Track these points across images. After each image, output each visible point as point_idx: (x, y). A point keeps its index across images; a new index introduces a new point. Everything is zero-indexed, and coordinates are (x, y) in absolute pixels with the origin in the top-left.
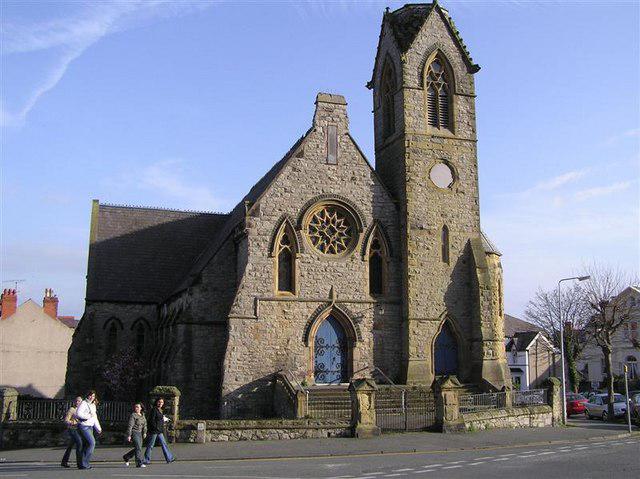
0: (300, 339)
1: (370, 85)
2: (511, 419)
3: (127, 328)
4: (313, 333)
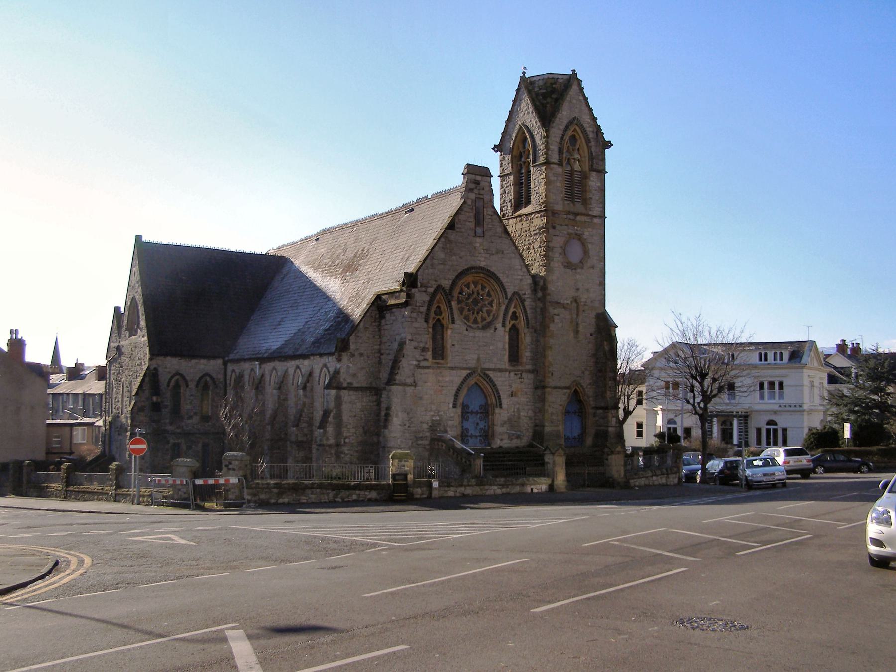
0: (451, 405)
1: (497, 148)
2: (654, 478)
3: (192, 385)
4: (460, 400)
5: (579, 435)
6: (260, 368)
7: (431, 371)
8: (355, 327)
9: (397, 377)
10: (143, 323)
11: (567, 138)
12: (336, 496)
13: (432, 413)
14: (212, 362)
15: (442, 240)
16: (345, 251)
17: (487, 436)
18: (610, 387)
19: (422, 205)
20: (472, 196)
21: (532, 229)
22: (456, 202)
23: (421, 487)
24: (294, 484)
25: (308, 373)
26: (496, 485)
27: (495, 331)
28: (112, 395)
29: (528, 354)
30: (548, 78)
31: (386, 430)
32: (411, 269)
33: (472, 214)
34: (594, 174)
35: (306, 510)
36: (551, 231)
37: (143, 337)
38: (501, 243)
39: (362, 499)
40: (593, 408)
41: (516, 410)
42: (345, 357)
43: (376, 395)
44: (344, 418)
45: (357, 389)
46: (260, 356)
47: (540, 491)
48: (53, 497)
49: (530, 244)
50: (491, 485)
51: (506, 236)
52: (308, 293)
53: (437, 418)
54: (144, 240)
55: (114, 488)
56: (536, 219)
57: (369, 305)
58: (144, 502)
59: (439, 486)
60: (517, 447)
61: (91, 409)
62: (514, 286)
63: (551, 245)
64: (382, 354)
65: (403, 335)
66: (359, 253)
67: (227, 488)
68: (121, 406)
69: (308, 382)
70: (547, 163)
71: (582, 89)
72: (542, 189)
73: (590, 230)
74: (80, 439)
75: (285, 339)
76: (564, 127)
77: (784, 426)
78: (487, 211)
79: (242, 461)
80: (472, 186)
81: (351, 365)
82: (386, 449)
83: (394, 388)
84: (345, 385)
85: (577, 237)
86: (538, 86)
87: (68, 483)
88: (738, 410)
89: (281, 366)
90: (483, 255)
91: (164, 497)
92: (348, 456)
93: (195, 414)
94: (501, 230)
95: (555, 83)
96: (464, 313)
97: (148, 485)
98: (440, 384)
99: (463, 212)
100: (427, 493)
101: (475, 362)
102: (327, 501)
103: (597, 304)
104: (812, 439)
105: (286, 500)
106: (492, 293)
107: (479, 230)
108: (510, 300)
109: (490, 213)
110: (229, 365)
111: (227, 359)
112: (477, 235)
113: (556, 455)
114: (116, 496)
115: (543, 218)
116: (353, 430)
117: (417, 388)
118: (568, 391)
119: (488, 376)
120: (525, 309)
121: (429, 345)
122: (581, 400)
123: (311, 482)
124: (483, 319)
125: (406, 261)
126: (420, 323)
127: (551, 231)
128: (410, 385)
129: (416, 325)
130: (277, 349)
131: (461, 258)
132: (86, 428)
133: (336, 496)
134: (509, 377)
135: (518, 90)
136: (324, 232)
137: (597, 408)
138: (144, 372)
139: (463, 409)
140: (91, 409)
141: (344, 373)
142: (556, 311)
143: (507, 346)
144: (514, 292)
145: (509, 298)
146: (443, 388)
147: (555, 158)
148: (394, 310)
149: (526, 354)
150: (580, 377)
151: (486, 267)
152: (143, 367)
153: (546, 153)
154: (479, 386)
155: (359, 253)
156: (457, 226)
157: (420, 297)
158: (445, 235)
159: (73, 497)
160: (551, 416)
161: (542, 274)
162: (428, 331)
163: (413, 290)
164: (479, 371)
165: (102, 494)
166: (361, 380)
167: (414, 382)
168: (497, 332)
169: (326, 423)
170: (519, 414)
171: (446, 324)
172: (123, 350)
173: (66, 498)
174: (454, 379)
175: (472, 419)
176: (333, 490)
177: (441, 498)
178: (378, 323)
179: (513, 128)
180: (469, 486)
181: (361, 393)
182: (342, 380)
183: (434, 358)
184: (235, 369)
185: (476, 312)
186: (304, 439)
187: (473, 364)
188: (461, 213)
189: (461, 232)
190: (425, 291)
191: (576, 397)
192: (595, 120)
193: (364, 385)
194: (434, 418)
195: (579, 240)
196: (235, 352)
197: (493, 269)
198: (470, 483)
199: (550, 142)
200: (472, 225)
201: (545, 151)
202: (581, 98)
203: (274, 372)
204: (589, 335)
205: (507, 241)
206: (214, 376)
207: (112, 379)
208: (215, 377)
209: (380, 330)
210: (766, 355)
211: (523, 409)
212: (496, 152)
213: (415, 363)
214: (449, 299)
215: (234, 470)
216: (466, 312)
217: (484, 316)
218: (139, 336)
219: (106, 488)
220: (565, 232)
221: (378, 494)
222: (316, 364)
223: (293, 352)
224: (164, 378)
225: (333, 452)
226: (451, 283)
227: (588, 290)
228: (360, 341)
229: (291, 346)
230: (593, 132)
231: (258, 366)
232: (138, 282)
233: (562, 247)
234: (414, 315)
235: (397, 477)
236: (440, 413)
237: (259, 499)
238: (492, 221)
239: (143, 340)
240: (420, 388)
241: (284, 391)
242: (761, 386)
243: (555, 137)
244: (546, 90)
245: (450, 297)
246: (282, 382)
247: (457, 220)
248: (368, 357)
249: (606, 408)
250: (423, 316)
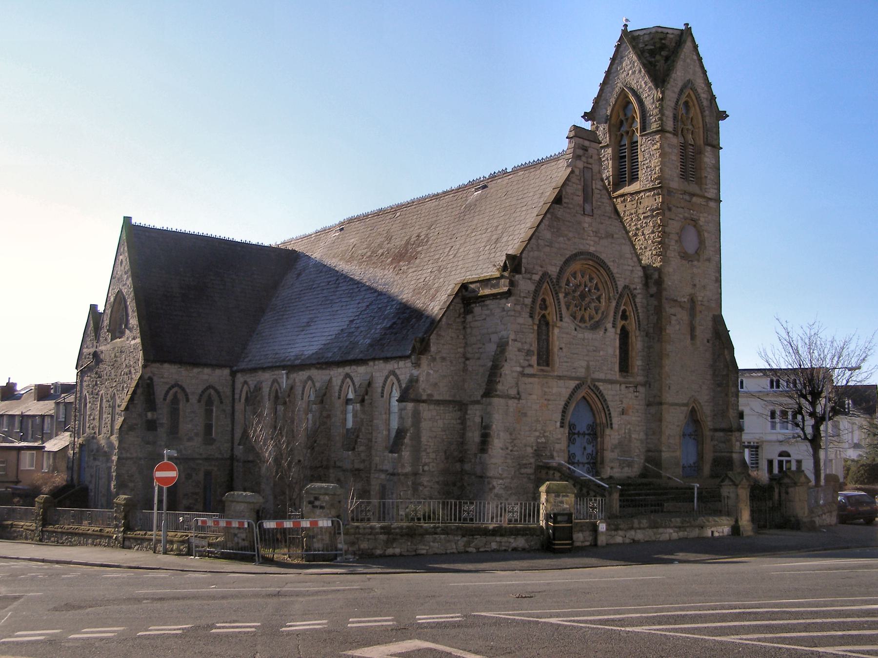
0: (558, 424)
3: (193, 399)
4: (568, 418)
5: (694, 463)
6: (288, 378)
7: (536, 380)
8: (433, 324)
9: (499, 387)
10: (134, 321)
11: (681, 102)
12: (468, 544)
13: (537, 434)
14: (218, 372)
15: (549, 216)
16: (389, 239)
17: (594, 463)
18: (732, 405)
19: (499, 180)
20: (580, 164)
21: (641, 211)
22: (560, 172)
23: (582, 531)
24: (408, 527)
25: (367, 382)
26: (671, 528)
27: (605, 333)
28: (85, 412)
29: (639, 363)
30: (657, 32)
31: (486, 455)
32: (513, 247)
33: (580, 187)
34: (709, 149)
35: (451, 566)
36: (667, 213)
37: (134, 339)
38: (611, 225)
39: (504, 548)
40: (711, 430)
41: (627, 431)
42: (424, 360)
43: (460, 410)
44: (422, 440)
45: (438, 403)
46: (289, 363)
47: (721, 534)
48: (20, 539)
49: (637, 229)
50: (666, 527)
51: (616, 217)
52: (343, 288)
53: (543, 440)
54: (133, 222)
55: (122, 529)
56: (646, 199)
57: (452, 297)
58: (172, 550)
59: (607, 529)
60: (629, 477)
61: (30, 432)
62: (625, 279)
63: (667, 229)
64: (467, 359)
65: (504, 333)
66: (413, 240)
67: (311, 534)
68: (98, 425)
69: (367, 394)
70: (662, 131)
71: (696, 47)
72: (655, 162)
73: (706, 215)
74: (27, 466)
75: (323, 342)
76: (679, 89)
77: (799, 457)
78: (596, 184)
79: (334, 494)
80: (580, 152)
81: (431, 372)
82: (486, 480)
83: (495, 401)
84: (424, 397)
85: (693, 222)
86: (644, 42)
87: (45, 522)
88: (749, 441)
89: (320, 376)
90: (593, 238)
91: (210, 545)
92: (427, 489)
93: (197, 435)
94: (610, 208)
95: (664, 39)
96: (570, 309)
97: (177, 527)
98: (546, 397)
99: (570, 184)
100: (590, 538)
101: (583, 370)
102: (455, 551)
103: (713, 305)
104: (863, 472)
105: (397, 551)
106: (600, 285)
107: (588, 207)
108: (621, 296)
109: (599, 187)
110: (239, 375)
111: (235, 368)
112: (586, 213)
113: (740, 487)
114: (124, 541)
115: (657, 197)
116: (432, 456)
117: (521, 401)
118: (684, 409)
119: (597, 388)
120: (636, 307)
121: (534, 348)
122: (698, 421)
123: (432, 525)
124: (591, 318)
125: (496, 242)
126: (524, 319)
127: (667, 213)
128: (513, 398)
129: (520, 320)
130: (313, 354)
131: (569, 240)
132: (35, 452)
133: (468, 544)
134: (620, 390)
135: (618, 47)
136: (351, 221)
137: (716, 430)
138: (134, 384)
139: (570, 428)
140: (30, 432)
141: (423, 381)
142: (672, 311)
143: (617, 352)
144: (625, 285)
145: (619, 292)
146: (550, 402)
147: (669, 125)
148: (488, 302)
149: (637, 362)
150: (698, 392)
151: (595, 253)
152: (134, 376)
153: (661, 119)
154: (588, 402)
155: (413, 240)
156: (564, 200)
157: (525, 285)
158: (551, 210)
159: (52, 539)
160: (668, 439)
161: (657, 264)
162: (533, 329)
163: (517, 276)
164: (589, 382)
165: (101, 537)
166: (443, 392)
167: (518, 394)
168: (608, 334)
169: (402, 445)
170: (630, 436)
171: (553, 321)
172: (102, 356)
173: (41, 541)
174: (562, 390)
175: (580, 441)
176: (463, 536)
177: (608, 545)
178: (463, 320)
179: (611, 93)
180: (640, 529)
181: (442, 408)
182: (421, 390)
183: (538, 364)
184: (248, 380)
185: (583, 309)
186: (362, 466)
187: (581, 372)
188: (568, 185)
189: (569, 208)
190: (530, 279)
191: (694, 417)
192: (709, 85)
193: (447, 398)
194: (539, 440)
195: (695, 226)
196: (247, 360)
197: (603, 256)
198: (642, 526)
199: (665, 106)
200: (580, 199)
201: (659, 116)
202: (695, 57)
203: (310, 382)
204: (706, 341)
205: (617, 223)
206: (220, 388)
207: (85, 392)
208: (221, 390)
209: (464, 328)
210: (778, 382)
211: (635, 431)
212: (586, 120)
213: (519, 369)
214: (556, 290)
215: (322, 507)
216: (572, 308)
217: (592, 314)
218: (128, 338)
219: (108, 530)
220: (681, 216)
221: (527, 541)
222: (379, 371)
223: (341, 357)
224: (160, 390)
225: (410, 483)
226: (558, 271)
227: (704, 287)
228: (442, 342)
229: (335, 351)
230: (707, 99)
231: (285, 376)
232: (126, 273)
233: (678, 234)
234: (518, 308)
235: (559, 518)
236: (546, 434)
237: (359, 549)
238: (601, 198)
239: (133, 342)
240: (524, 401)
241: (327, 406)
242: (773, 414)
243: (670, 100)
244: (655, 46)
245: (557, 288)
246: (325, 395)
247: (564, 193)
248: (451, 362)
249: (730, 430)
250: (528, 310)
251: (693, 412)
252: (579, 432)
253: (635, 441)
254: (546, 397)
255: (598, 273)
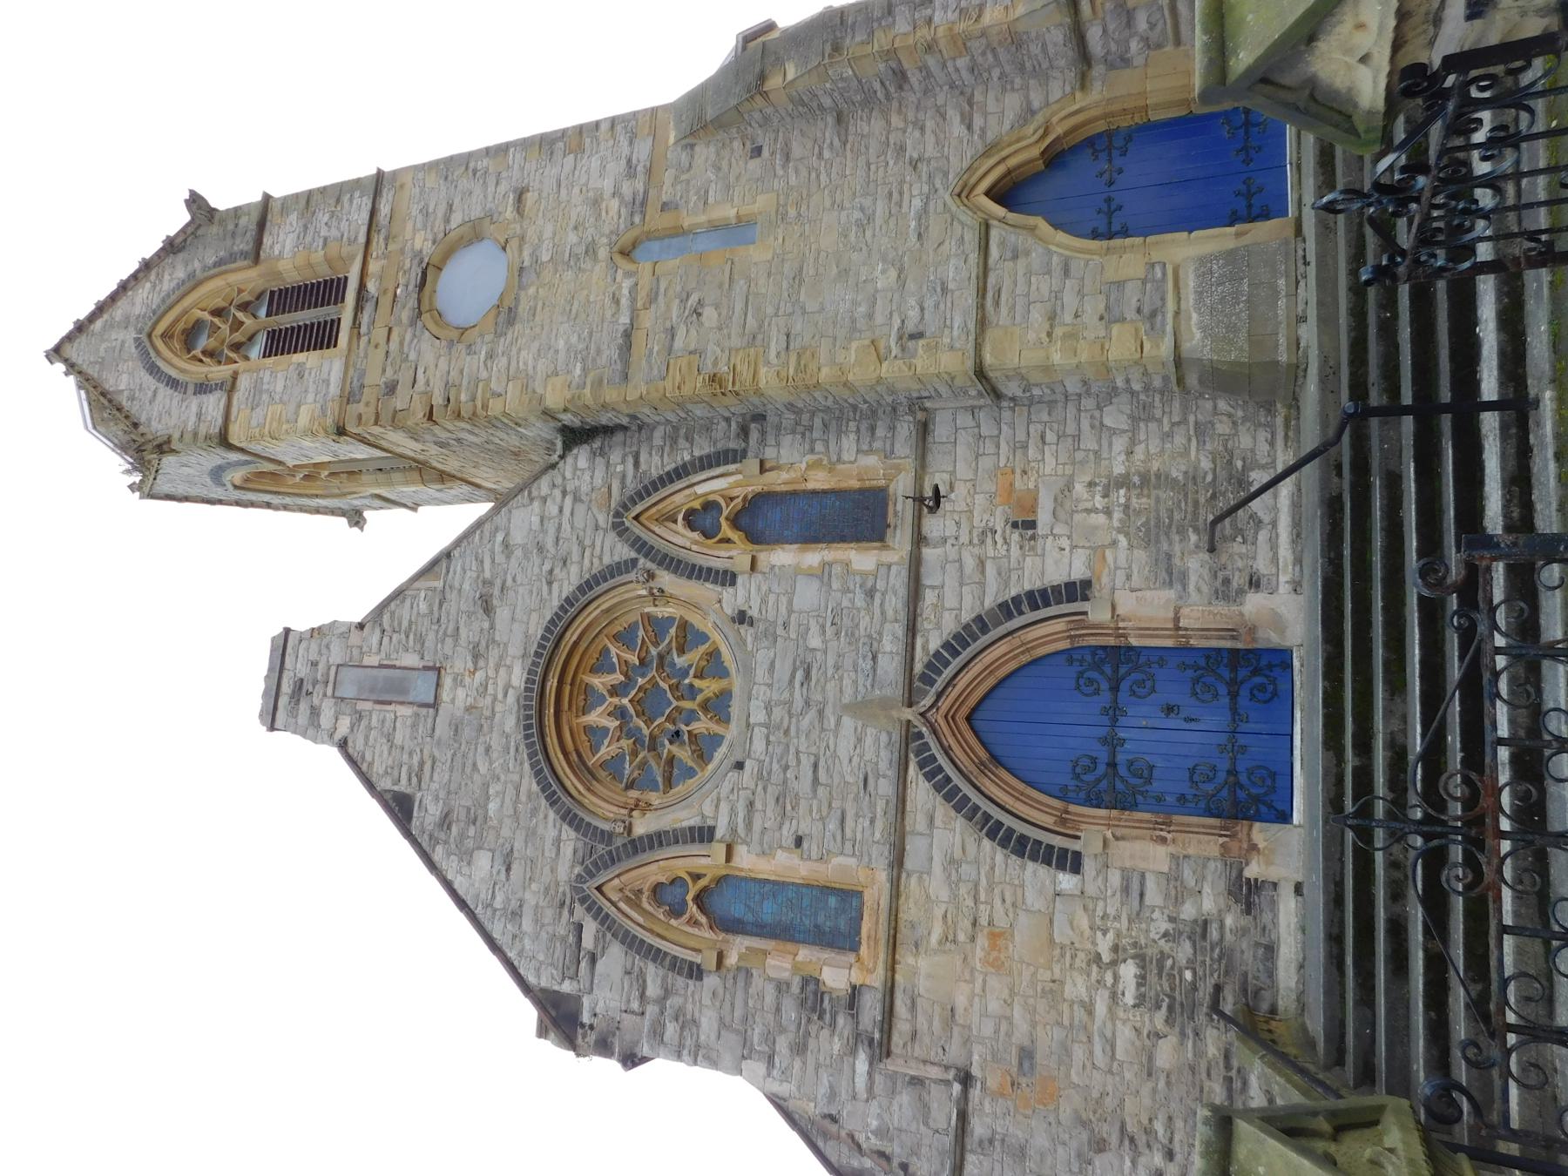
0: (1067, 881)
53: (1129, 971)
146: (984, 921)
236: (1106, 957)
251: (1008, 193)
252: (1104, 741)
253: (1140, 451)
254: (962, 937)
255: (583, 645)
